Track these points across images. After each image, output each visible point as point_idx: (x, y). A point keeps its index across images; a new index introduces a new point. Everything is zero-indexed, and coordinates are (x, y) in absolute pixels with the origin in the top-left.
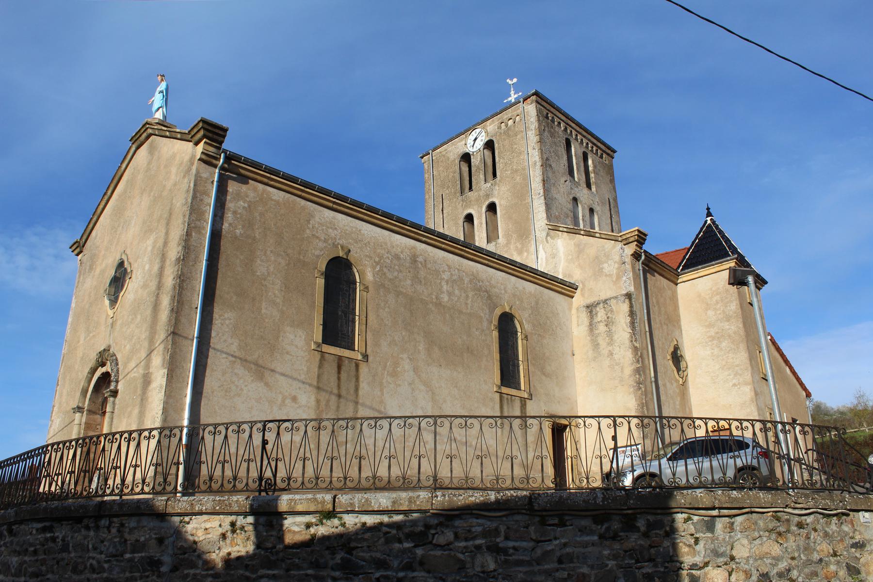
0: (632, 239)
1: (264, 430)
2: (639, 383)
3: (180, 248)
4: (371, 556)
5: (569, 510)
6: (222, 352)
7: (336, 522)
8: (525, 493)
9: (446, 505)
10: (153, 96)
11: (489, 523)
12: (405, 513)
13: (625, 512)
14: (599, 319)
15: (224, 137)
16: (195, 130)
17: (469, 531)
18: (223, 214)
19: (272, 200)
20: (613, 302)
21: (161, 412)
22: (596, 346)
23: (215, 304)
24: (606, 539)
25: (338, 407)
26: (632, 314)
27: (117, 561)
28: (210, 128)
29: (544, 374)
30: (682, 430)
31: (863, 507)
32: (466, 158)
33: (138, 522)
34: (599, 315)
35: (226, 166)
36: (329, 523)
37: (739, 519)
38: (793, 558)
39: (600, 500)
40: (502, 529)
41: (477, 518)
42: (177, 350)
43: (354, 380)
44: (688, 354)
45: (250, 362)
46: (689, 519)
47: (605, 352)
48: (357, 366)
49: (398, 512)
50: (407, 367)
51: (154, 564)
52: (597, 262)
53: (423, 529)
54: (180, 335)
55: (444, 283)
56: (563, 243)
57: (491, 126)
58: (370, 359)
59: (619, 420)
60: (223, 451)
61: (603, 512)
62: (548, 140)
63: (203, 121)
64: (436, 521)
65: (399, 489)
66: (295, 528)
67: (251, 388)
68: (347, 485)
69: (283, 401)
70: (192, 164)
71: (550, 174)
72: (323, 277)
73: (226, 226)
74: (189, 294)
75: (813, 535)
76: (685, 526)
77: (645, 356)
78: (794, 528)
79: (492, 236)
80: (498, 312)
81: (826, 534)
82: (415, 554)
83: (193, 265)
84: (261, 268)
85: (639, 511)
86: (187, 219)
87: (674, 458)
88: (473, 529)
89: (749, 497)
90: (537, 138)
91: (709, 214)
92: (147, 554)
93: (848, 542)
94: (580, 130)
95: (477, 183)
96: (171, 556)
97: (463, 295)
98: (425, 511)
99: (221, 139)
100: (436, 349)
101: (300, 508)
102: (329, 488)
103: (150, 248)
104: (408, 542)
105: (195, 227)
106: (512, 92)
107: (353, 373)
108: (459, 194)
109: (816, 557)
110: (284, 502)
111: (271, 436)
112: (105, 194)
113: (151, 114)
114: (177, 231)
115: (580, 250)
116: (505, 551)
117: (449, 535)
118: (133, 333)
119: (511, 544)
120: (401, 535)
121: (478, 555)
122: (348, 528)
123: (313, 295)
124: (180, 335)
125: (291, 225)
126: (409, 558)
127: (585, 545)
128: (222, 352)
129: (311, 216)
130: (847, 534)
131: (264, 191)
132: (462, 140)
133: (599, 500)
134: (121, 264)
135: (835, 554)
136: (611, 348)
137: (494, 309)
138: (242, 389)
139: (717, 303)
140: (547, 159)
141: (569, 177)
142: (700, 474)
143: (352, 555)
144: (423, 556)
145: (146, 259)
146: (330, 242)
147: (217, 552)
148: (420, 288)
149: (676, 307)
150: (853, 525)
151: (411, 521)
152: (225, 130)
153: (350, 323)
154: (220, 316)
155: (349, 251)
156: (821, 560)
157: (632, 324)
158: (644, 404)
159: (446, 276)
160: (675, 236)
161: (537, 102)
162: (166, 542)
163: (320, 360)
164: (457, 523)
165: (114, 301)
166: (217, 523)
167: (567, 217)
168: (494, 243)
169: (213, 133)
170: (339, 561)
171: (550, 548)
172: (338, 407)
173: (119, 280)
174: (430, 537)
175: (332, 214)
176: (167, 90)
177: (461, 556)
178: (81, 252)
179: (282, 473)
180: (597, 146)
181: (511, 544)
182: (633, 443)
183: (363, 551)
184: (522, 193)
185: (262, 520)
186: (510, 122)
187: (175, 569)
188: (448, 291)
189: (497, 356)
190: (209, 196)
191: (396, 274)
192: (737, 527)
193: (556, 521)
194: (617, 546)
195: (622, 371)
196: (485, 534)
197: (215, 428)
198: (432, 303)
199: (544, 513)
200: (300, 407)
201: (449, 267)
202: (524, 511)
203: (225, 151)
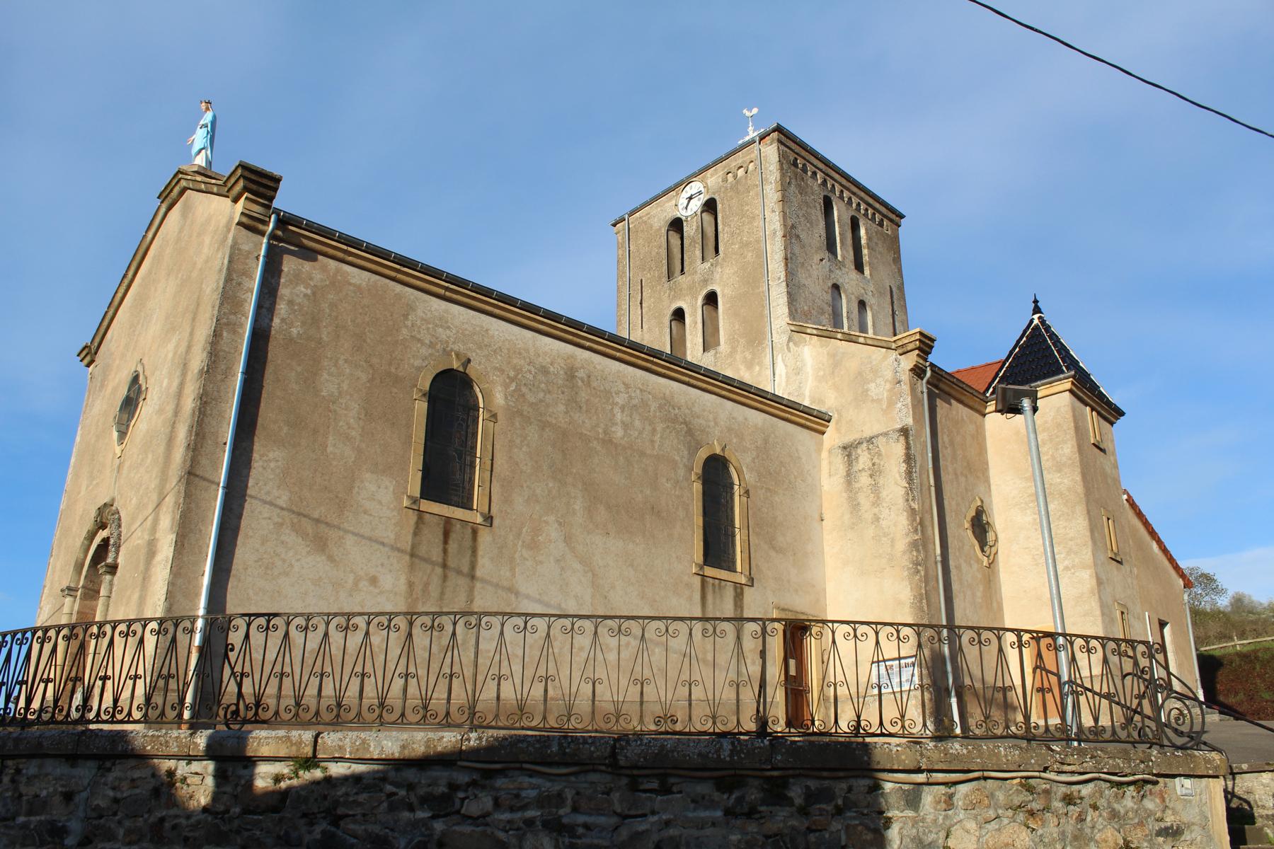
0: (911, 346)
2: (917, 564)
3: (205, 354)
4: (366, 830)
11: (548, 784)
13: (768, 773)
14: (861, 466)
15: (276, 190)
16: (233, 180)
17: (517, 796)
18: (274, 303)
19: (350, 284)
20: (882, 440)
22: (855, 507)
24: (736, 816)
25: (442, 593)
26: (909, 458)
27: (6, 826)
28: (253, 177)
29: (774, 548)
31: (1181, 771)
34: (861, 460)
35: (279, 233)
37: (963, 789)
39: (727, 753)
40: (569, 794)
41: (531, 776)
42: (193, 505)
43: (469, 553)
44: (1000, 519)
47: (868, 516)
48: (475, 533)
50: (554, 535)
51: (58, 832)
52: (861, 379)
55: (617, 410)
56: (812, 352)
57: (714, 178)
58: (496, 522)
59: (770, 627)
60: (280, 659)
61: (732, 772)
62: (796, 199)
63: (243, 166)
67: (308, 564)
69: (356, 584)
70: (229, 230)
71: (797, 249)
72: (425, 399)
75: (1091, 815)
77: (927, 523)
78: (1057, 804)
79: (709, 343)
80: (703, 454)
81: (1114, 815)
83: (223, 381)
84: (328, 385)
85: (791, 772)
86: (216, 312)
88: (524, 794)
89: (981, 755)
90: (778, 196)
91: (1037, 310)
92: (48, 817)
95: (691, 263)
97: (648, 428)
99: (270, 193)
100: (602, 509)
103: (170, 355)
105: (228, 324)
106: (751, 129)
107: (468, 542)
112: (125, 276)
113: (190, 158)
114: (204, 331)
115: (836, 362)
116: (571, 830)
117: (486, 802)
118: (134, 474)
119: (581, 819)
120: (413, 799)
127: (701, 825)
129: (411, 308)
130: (1150, 814)
131: (338, 271)
132: (670, 200)
134: (135, 379)
136: (876, 510)
137: (697, 450)
138: (291, 565)
140: (793, 227)
141: (827, 255)
143: (338, 826)
144: (443, 833)
145: (165, 371)
146: (438, 347)
147: (146, 816)
149: (982, 450)
150: (1163, 800)
152: (277, 180)
154: (262, 456)
155: (469, 361)
157: (909, 473)
158: (924, 598)
159: (620, 400)
160: (981, 342)
161: (780, 141)
162: (77, 799)
164: (500, 782)
165: (122, 435)
167: (823, 313)
168: (712, 352)
169: (259, 184)
170: (319, 837)
172: (442, 593)
173: (130, 404)
174: (458, 802)
175: (444, 305)
176: (214, 123)
177: (501, 835)
180: (874, 208)
181: (581, 819)
184: (754, 277)
186: (741, 172)
187: (87, 840)
188: (623, 422)
189: (698, 520)
190: (252, 278)
191: (541, 395)
192: (959, 801)
193: (655, 785)
194: (752, 827)
195: (892, 546)
196: (541, 802)
197: (308, 620)
199: (635, 772)
200: (381, 593)
201: (627, 386)
202: (603, 768)
203: (277, 211)
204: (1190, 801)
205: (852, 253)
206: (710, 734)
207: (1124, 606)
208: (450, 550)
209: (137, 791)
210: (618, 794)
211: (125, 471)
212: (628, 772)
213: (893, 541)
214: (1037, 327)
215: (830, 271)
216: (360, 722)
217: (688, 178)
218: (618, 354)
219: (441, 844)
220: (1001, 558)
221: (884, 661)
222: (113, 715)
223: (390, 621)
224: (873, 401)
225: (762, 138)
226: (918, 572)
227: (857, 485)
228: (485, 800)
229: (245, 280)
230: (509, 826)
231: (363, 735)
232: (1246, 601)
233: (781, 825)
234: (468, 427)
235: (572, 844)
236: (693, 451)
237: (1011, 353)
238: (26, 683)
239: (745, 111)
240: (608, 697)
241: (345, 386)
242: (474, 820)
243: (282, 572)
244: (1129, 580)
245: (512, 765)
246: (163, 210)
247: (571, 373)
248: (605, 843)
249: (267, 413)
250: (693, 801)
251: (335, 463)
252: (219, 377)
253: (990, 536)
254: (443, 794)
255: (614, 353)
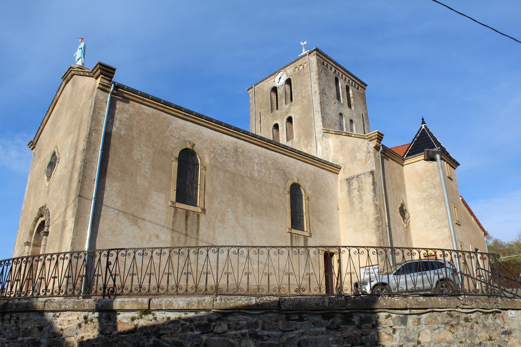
0: (374, 138)
1: (108, 256)
2: (378, 227)
3: (85, 143)
4: (172, 340)
5: (306, 310)
6: (110, 208)
7: (151, 316)
8: (276, 298)
9: (223, 307)
10: (76, 51)
11: (251, 318)
12: (196, 311)
13: (345, 311)
14: (354, 187)
15: (113, 74)
16: (95, 70)
17: (238, 324)
19: (145, 113)
20: (363, 176)
21: (70, 245)
22: (352, 204)
23: (107, 178)
24: (331, 330)
26: (374, 184)
27: (13, 342)
28: (104, 68)
29: (319, 221)
30: (403, 257)
32: (274, 90)
33: (28, 316)
34: (354, 185)
35: (115, 92)
36: (146, 317)
37: (424, 316)
38: (461, 342)
39: (327, 303)
40: (260, 322)
41: (243, 315)
42: (82, 206)
43: (196, 224)
44: (410, 208)
45: (129, 214)
46: (389, 316)
47: (358, 208)
48: (198, 216)
49: (191, 311)
52: (353, 151)
53: (207, 322)
54: (83, 197)
55: (255, 165)
56: (332, 141)
57: (290, 70)
58: (207, 212)
59: (342, 249)
61: (329, 311)
63: (100, 64)
64: (216, 317)
65: (193, 294)
66: (125, 321)
68: (159, 291)
69: (150, 238)
70: (94, 91)
71: (325, 99)
72: (177, 161)
73: (114, 129)
74: (90, 171)
75: (475, 326)
76: (386, 321)
77: (382, 210)
78: (462, 322)
80: (290, 183)
81: (485, 326)
82: (202, 339)
83: (93, 153)
84: (137, 155)
85: (354, 311)
86: (89, 125)
87: (398, 273)
89: (431, 302)
90: (317, 77)
91: (423, 123)
92: (32, 337)
93: (500, 330)
94: (345, 72)
95: (281, 105)
96: (47, 339)
97: (268, 172)
98: (209, 310)
99: (111, 75)
101: (127, 307)
102: (148, 294)
103: (69, 144)
104: (196, 330)
105: (95, 130)
106: (304, 50)
107: (195, 220)
108: (270, 112)
109: (477, 341)
110: (117, 303)
111: (112, 259)
112: (48, 112)
113: (75, 62)
114: (84, 133)
115: (342, 145)
116: (261, 337)
117: (225, 327)
118: (56, 194)
119: (266, 333)
120: (193, 326)
121: (244, 340)
122: (158, 321)
123: (170, 172)
124: (83, 197)
125: (159, 129)
126: (198, 341)
127: (317, 334)
128: (110, 208)
129: (170, 123)
130: (499, 325)
131: (140, 107)
132: (272, 79)
133: (326, 304)
134: (54, 154)
135: (490, 339)
136: (361, 205)
137: (288, 181)
139: (428, 177)
140: (323, 89)
141: (337, 101)
142: (398, 286)
143: (160, 339)
144: (206, 340)
145: (67, 150)
146: (182, 139)
147: (75, 336)
148: (239, 168)
150: (503, 320)
151: (200, 317)
152: (114, 70)
153: (194, 190)
154: (110, 185)
155: (194, 145)
156: (481, 343)
157: (374, 190)
159: (256, 160)
160: (400, 138)
161: (317, 55)
162: (44, 329)
163: (174, 212)
164: (230, 318)
165: (49, 178)
166: (76, 317)
167: (336, 125)
168: (291, 141)
169: (106, 71)
170: (152, 343)
171: (292, 336)
173: (52, 165)
174: (212, 327)
175: (184, 122)
176: (85, 47)
177: (232, 341)
178: (34, 148)
179: (118, 283)
180: (355, 82)
181: (266, 333)
182: (370, 264)
183: (168, 337)
184: (307, 110)
185: (104, 315)
186: (301, 68)
189: (289, 210)
191: (224, 159)
192: (423, 321)
194: (338, 334)
195: (368, 219)
196: (249, 326)
198: (247, 177)
199: (288, 312)
200: (160, 242)
201: (259, 155)
202: (275, 311)
203: (114, 83)
204: (514, 320)
205: (347, 100)
206: (319, 296)
207: (462, 243)
208: (188, 223)
209: (71, 325)
210: (281, 322)
211: (50, 193)
212: (286, 312)
213: (368, 217)
214: (424, 130)
215: (338, 108)
216: (167, 294)
217: (279, 70)
218: (255, 142)
219: (205, 345)
220: (411, 224)
221: (372, 266)
222: (59, 294)
223: (179, 250)
224: (358, 160)
225: (310, 53)
226: (379, 230)
227: (353, 195)
228: (224, 326)
229: (101, 111)
230: (235, 337)
231: (170, 299)
232: (499, 242)
233: (350, 333)
234: (194, 172)
235: (262, 344)
236: (286, 181)
237: (413, 140)
238: (20, 280)
239: (301, 43)
240: (254, 283)
241: (144, 156)
242: (219, 334)
243: (117, 233)
244: (463, 232)
245: (235, 311)
246: (64, 84)
247: (236, 150)
248: (276, 343)
249: (111, 166)
250: (313, 324)
251: (140, 188)
252: (91, 152)
253: (407, 215)
254: (206, 323)
255: (251, 140)
